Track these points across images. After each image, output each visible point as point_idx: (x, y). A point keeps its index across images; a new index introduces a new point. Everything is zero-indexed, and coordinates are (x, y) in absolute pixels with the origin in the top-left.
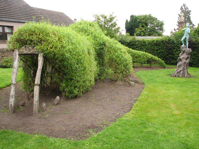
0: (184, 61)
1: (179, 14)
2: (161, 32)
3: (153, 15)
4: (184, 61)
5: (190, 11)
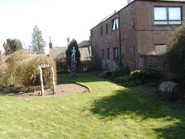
0: (75, 68)
1: (32, 34)
2: (137, 111)
3: (95, 23)
4: (75, 68)
5: (41, 31)
